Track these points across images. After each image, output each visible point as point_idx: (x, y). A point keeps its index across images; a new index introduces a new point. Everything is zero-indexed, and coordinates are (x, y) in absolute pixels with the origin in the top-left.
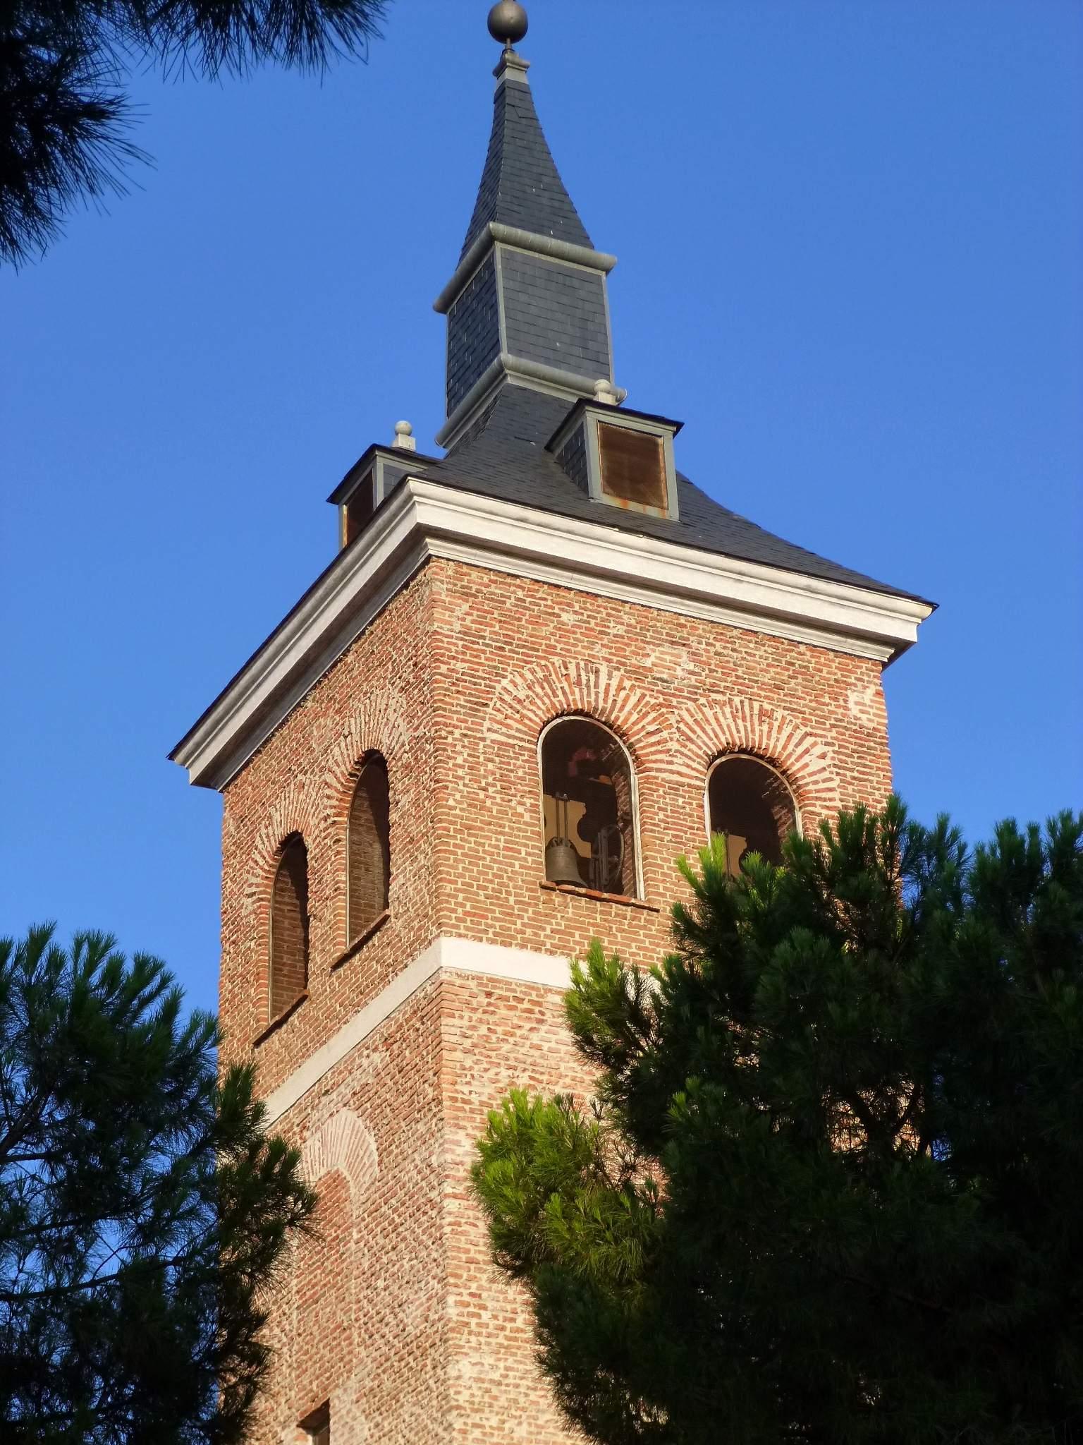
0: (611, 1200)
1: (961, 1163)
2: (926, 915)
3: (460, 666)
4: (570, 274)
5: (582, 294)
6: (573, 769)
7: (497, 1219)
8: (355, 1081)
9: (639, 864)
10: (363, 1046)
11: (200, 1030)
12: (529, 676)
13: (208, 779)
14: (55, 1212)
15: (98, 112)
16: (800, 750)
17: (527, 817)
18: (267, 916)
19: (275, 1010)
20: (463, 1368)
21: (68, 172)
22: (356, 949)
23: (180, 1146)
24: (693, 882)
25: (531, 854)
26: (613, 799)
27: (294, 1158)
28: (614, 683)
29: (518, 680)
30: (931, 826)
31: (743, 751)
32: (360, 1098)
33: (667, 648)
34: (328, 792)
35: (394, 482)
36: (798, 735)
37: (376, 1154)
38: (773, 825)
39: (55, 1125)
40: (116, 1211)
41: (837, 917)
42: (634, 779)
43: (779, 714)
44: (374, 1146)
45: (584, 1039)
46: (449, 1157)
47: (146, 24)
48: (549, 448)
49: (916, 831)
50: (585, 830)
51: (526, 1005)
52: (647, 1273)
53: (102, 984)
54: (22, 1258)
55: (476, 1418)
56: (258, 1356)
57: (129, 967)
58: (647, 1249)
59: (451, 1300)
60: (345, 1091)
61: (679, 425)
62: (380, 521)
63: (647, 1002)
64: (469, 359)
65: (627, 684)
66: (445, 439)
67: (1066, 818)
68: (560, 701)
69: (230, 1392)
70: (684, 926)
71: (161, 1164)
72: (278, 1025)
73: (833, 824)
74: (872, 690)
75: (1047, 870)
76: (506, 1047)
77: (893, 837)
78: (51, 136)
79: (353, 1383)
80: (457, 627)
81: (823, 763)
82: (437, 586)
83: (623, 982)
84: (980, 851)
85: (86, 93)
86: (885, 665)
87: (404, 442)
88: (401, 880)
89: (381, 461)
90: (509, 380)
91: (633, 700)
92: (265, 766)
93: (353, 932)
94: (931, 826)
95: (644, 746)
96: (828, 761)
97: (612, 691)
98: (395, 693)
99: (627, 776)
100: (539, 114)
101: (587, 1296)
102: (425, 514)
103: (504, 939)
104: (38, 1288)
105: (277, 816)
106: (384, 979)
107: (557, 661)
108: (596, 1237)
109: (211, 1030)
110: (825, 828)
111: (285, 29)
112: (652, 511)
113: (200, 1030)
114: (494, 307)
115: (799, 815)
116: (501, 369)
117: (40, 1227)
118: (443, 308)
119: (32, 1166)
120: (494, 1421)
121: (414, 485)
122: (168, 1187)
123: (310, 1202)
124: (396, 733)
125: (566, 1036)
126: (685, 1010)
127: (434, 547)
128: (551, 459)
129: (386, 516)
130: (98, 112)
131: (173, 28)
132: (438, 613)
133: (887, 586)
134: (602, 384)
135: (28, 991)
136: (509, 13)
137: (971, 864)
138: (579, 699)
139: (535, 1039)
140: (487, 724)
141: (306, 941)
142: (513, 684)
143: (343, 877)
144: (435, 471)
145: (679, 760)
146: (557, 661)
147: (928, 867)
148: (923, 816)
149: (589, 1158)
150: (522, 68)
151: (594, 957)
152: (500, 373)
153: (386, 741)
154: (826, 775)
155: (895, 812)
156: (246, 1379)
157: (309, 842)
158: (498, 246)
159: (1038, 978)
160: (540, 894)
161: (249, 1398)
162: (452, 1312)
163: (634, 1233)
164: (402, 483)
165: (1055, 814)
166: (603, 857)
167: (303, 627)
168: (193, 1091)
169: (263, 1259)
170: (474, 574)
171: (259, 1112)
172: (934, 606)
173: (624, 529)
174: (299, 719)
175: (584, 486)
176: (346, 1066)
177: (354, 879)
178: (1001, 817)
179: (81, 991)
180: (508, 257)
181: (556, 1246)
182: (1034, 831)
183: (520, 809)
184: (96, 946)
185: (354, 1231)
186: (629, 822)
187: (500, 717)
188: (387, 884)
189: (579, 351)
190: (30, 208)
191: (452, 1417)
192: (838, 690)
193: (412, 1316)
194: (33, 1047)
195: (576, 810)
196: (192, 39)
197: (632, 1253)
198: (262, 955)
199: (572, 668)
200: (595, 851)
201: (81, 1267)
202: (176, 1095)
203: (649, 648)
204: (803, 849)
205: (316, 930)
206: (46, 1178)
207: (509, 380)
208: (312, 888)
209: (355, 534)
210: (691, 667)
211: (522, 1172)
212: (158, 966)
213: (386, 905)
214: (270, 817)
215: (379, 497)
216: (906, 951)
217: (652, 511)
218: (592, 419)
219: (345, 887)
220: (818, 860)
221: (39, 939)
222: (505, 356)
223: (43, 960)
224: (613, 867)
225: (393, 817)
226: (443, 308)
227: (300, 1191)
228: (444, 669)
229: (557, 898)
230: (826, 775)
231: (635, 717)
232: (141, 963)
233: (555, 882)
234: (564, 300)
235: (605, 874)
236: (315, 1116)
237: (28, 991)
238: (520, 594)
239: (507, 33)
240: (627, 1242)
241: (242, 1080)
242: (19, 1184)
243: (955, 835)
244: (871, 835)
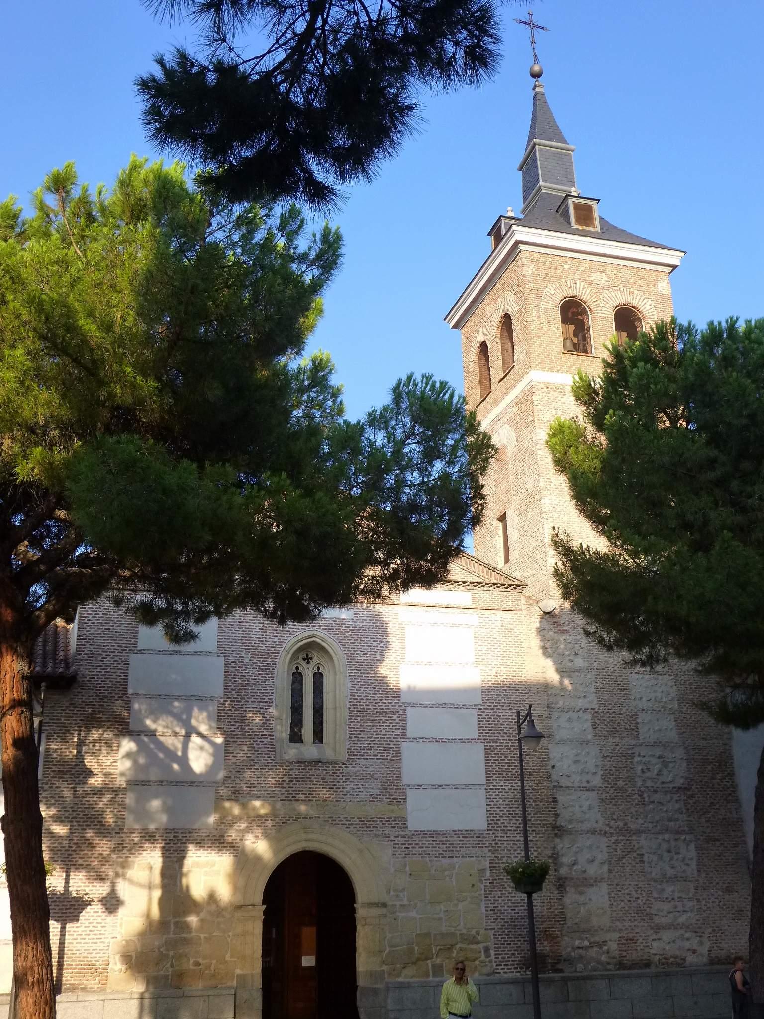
0: (590, 448)
1: (699, 430)
2: (685, 354)
3: (532, 285)
4: (558, 153)
5: (565, 160)
6: (570, 315)
7: (554, 456)
8: (508, 416)
9: (593, 343)
10: (509, 406)
11: (461, 399)
12: (554, 286)
13: (456, 327)
14: (421, 459)
15: (410, 108)
16: (643, 303)
17: (556, 331)
18: (477, 366)
19: (482, 396)
20: (546, 501)
21: (403, 129)
22: (505, 376)
23: (457, 436)
24: (608, 350)
25: (559, 342)
26: (584, 324)
27: (490, 438)
29: (551, 287)
30: (686, 324)
31: (625, 305)
32: (510, 422)
33: (599, 273)
35: (508, 228)
36: (642, 298)
38: (635, 328)
39: (420, 433)
40: (439, 458)
41: (656, 355)
42: (590, 317)
43: (636, 292)
44: (514, 435)
45: (578, 399)
46: (538, 438)
47: (424, 77)
48: (557, 212)
49: (681, 326)
50: (575, 334)
51: (559, 390)
52: (603, 469)
53: (430, 390)
54: (412, 473)
55: (550, 515)
56: (483, 497)
57: (438, 385)
58: (602, 462)
59: (541, 480)
60: (505, 419)
61: (599, 200)
62: (504, 240)
63: (598, 386)
64: (529, 185)
66: (523, 212)
67: (731, 318)
68: (565, 294)
69: (477, 509)
70: (607, 365)
71: (450, 442)
72: (483, 401)
73: (654, 326)
74: (666, 281)
75: (725, 336)
76: (553, 403)
77: (674, 329)
78: (397, 118)
79: (513, 507)
80: (531, 272)
81: (651, 307)
82: (524, 260)
83: (590, 382)
84: (702, 332)
85: (406, 102)
86: (670, 273)
87: (510, 214)
88: (518, 354)
89: (503, 221)
90: (543, 191)
92: (473, 321)
93: (504, 371)
94: (686, 324)
95: (593, 306)
96: (652, 306)
97: (581, 289)
98: (512, 295)
99: (588, 316)
100: (548, 101)
101: (584, 476)
102: (518, 237)
103: (551, 370)
104: (418, 482)
105: (478, 337)
106: (515, 385)
107: (563, 280)
108: (586, 459)
109: (465, 401)
110: (651, 328)
111: (468, 75)
112: (591, 229)
113: (461, 399)
114: (536, 167)
115: (643, 324)
116: (540, 187)
117: (417, 465)
118: (520, 169)
119: (414, 446)
120: (556, 516)
121: (514, 228)
122: (454, 448)
123: (496, 451)
125: (573, 399)
126: (610, 389)
127: (522, 247)
128: (558, 215)
129: (506, 238)
130: (410, 108)
131: (432, 77)
132: (524, 268)
134: (573, 189)
135: (408, 393)
136: (536, 68)
137: (699, 338)
138: (571, 292)
139: (562, 400)
140: (542, 303)
141: (490, 374)
142: (550, 289)
143: (500, 354)
144: (520, 222)
145: (605, 309)
146: (563, 280)
147: (686, 337)
148: (683, 321)
149: (582, 436)
150: (542, 86)
151: (579, 374)
152: (540, 188)
153: (510, 311)
154: (652, 310)
155: (673, 321)
156: (481, 504)
157: (488, 344)
158: (537, 146)
159: (723, 370)
160: (563, 355)
161: (482, 510)
162: (542, 484)
163: (597, 457)
164: (510, 227)
165: (727, 317)
166: (581, 342)
168: (459, 420)
169: (484, 469)
170: (535, 255)
171: (479, 425)
172: (685, 253)
173: (582, 236)
174: (483, 305)
175: (569, 223)
176: (504, 412)
177: (503, 354)
178: (708, 320)
179: (423, 393)
180: (540, 150)
181: (573, 463)
182: (720, 323)
183: (554, 329)
184: (428, 378)
186: (589, 331)
187: (546, 300)
188: (514, 356)
189: (564, 179)
190: (392, 142)
191: (543, 515)
192: (655, 282)
193: (529, 486)
194: (411, 411)
195: (572, 328)
196: (439, 80)
197: (597, 463)
198: (476, 379)
199: (568, 282)
200: (578, 341)
201: (430, 474)
202: (455, 421)
203: (593, 274)
204: (644, 335)
205: (492, 371)
206: (418, 450)
207: (543, 191)
208: (490, 358)
209: (496, 246)
210: (607, 279)
211: (561, 441)
212: (447, 383)
213: (514, 362)
215: (503, 233)
216: (680, 364)
217: (591, 229)
218: (570, 201)
219: (501, 357)
220: (650, 338)
221: (410, 377)
222: (541, 183)
223: (412, 384)
224: (585, 345)
225: (514, 334)
227: (493, 448)
228: (527, 286)
229: (567, 356)
230: (652, 310)
231: (589, 297)
232: (441, 383)
233: (566, 351)
234: (560, 162)
235: (582, 347)
236: (496, 428)
237: (408, 393)
238: (550, 260)
239: (536, 75)
240: (596, 460)
241: (473, 415)
242: (410, 452)
243: (694, 327)
244: (666, 329)
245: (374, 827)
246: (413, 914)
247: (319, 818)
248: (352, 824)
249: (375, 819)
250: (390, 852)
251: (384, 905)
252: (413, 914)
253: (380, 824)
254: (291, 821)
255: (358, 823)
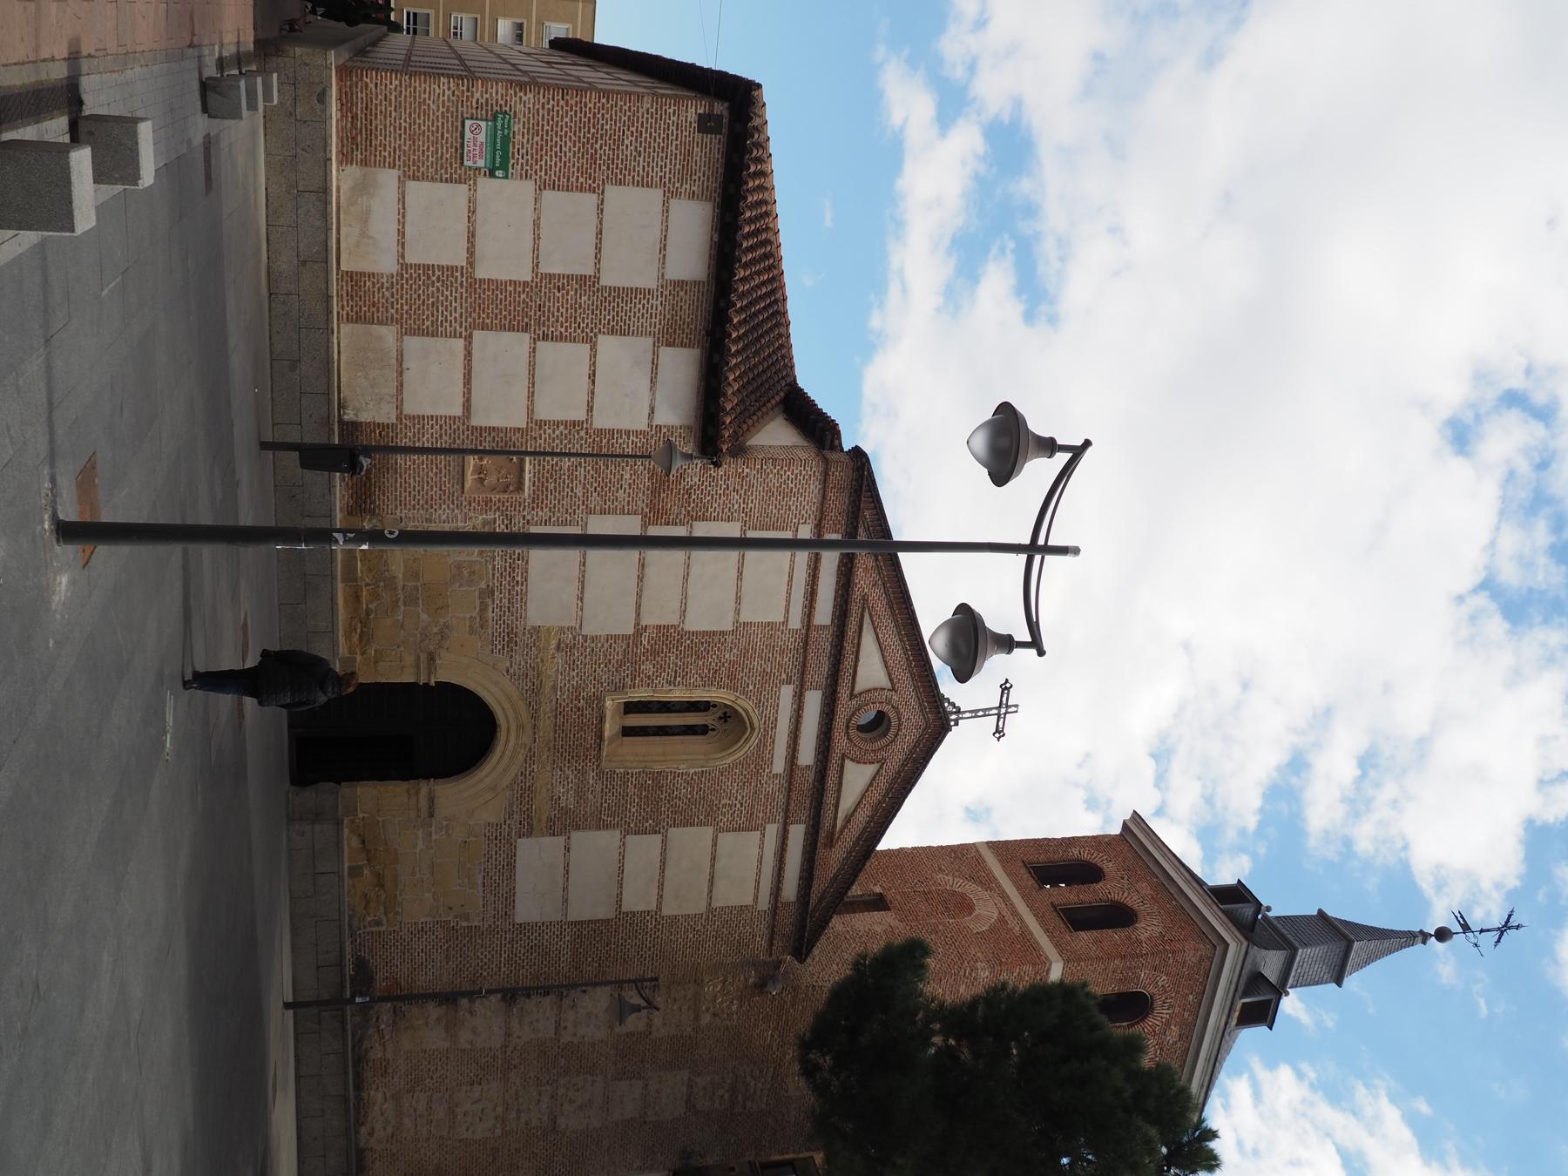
28: (1165, 1016)
34: (1121, 893)
37: (981, 930)
65: (1164, 1020)
91: (1157, 1023)
124: (1144, 931)
133: (1221, 1065)
167: (1187, 882)
175: (1245, 995)
176: (1015, 913)
185: (953, 920)
210: (1171, 1042)
214: (1110, 861)
226: (1321, 913)
231: (1150, 1024)
245: (521, 801)
246: (421, 845)
247: (535, 742)
248: (525, 778)
249: (531, 803)
250: (493, 820)
251: (431, 815)
252: (421, 845)
253: (525, 809)
254: (532, 712)
255: (528, 784)
